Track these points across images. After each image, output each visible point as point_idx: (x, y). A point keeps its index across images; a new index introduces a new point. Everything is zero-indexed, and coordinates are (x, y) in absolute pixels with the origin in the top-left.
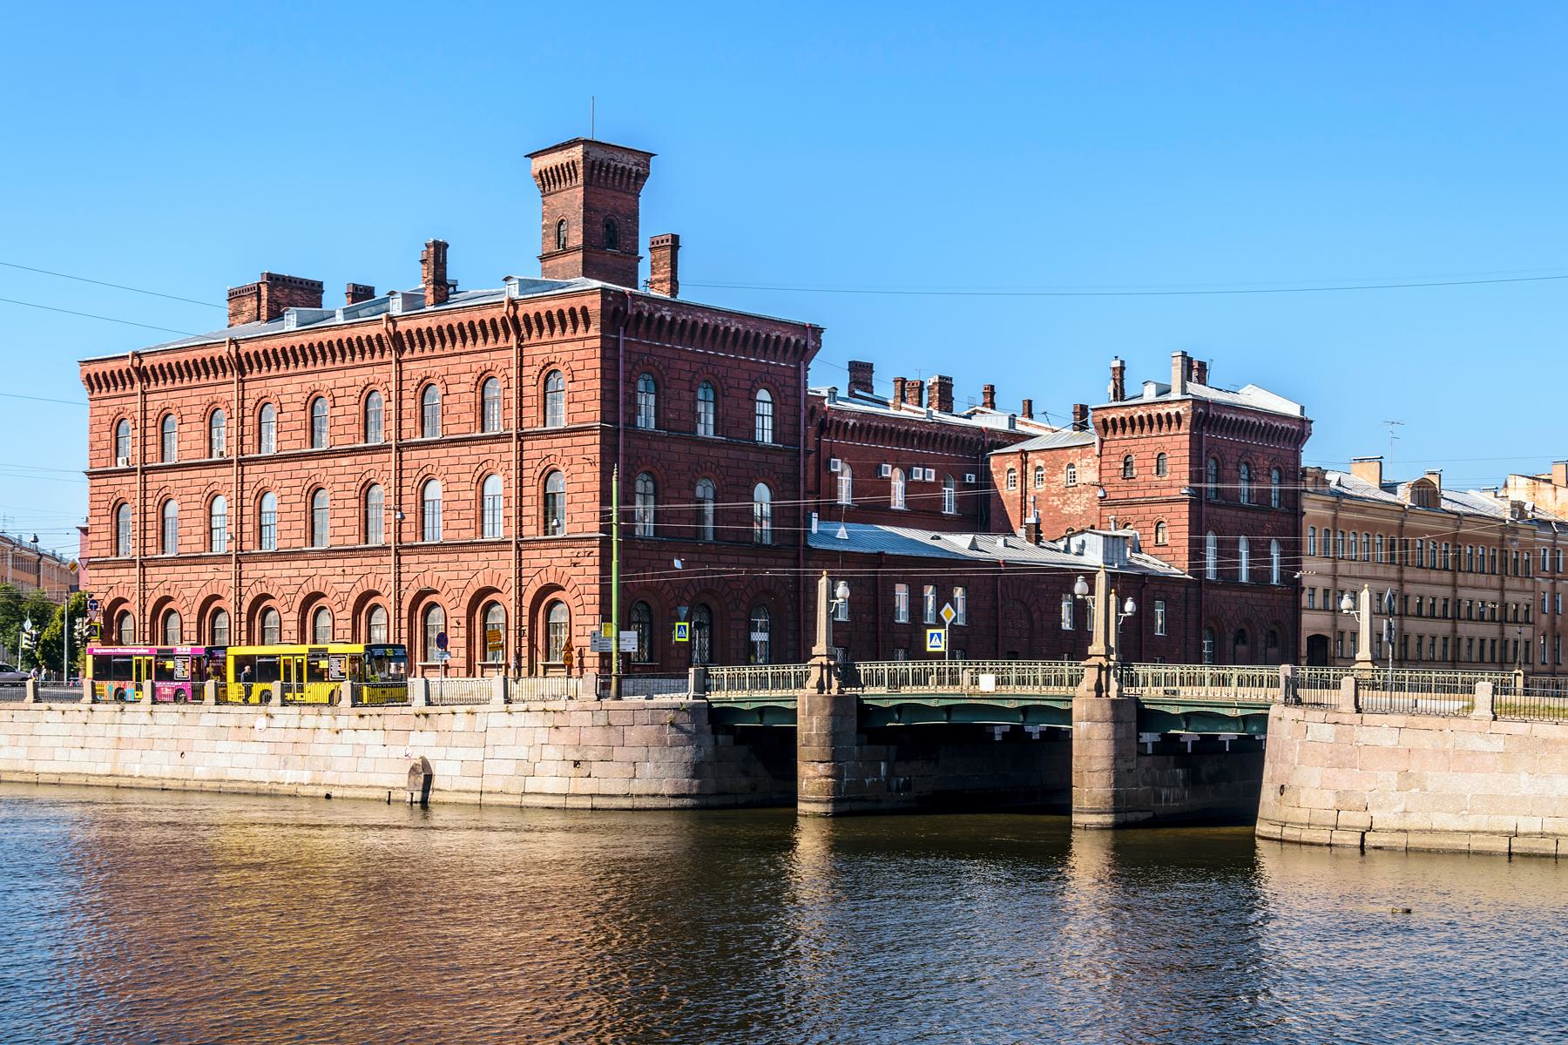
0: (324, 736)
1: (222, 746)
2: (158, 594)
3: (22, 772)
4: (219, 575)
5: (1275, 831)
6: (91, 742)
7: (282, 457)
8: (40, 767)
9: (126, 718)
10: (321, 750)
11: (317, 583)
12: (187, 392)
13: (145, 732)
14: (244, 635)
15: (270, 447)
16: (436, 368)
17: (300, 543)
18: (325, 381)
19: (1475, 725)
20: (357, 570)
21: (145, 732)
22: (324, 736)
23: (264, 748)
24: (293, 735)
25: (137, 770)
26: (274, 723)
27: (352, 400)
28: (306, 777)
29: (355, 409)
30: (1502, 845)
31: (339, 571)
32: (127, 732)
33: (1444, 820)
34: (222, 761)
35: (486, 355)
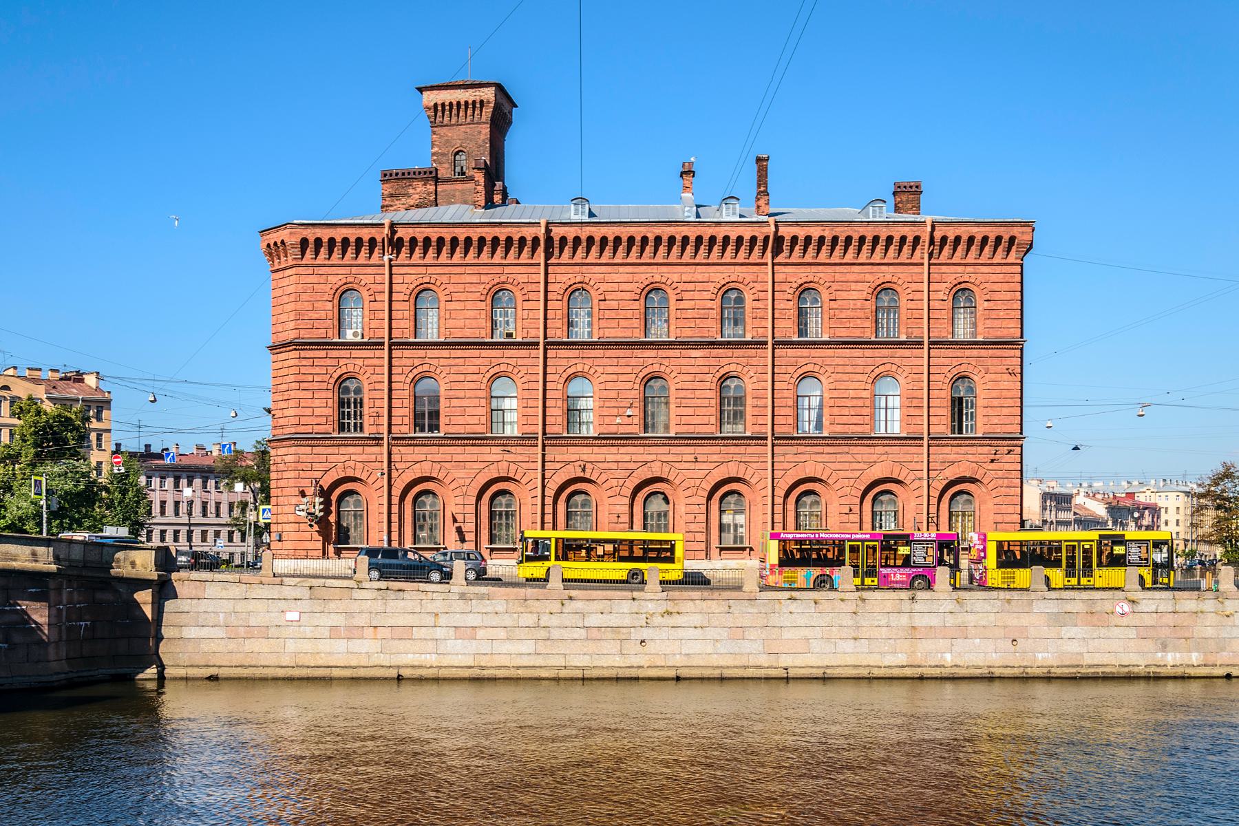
0: (1211, 619)
1: (1068, 632)
2: (408, 477)
3: (760, 667)
4: (507, 457)
5: (182, 672)
6: (864, 633)
7: (603, 344)
8: (785, 661)
9: (917, 607)
10: (1210, 632)
11: (750, 471)
12: (458, 270)
13: (950, 621)
14: (549, 518)
15: (431, 332)
16: (820, 276)
17: (636, 430)
18: (669, 275)
19: (941, 596)
20: (715, 458)
21: (950, 621)
22: (1211, 619)
23: (1132, 633)
24: (1170, 619)
25: (948, 659)
26: (1139, 608)
27: (791, 291)
28: (1195, 658)
29: (329, 306)
30: (393, 673)
31: (691, 458)
32: (920, 621)
33: (1106, 659)
34: (1074, 647)
35: (422, 270)
